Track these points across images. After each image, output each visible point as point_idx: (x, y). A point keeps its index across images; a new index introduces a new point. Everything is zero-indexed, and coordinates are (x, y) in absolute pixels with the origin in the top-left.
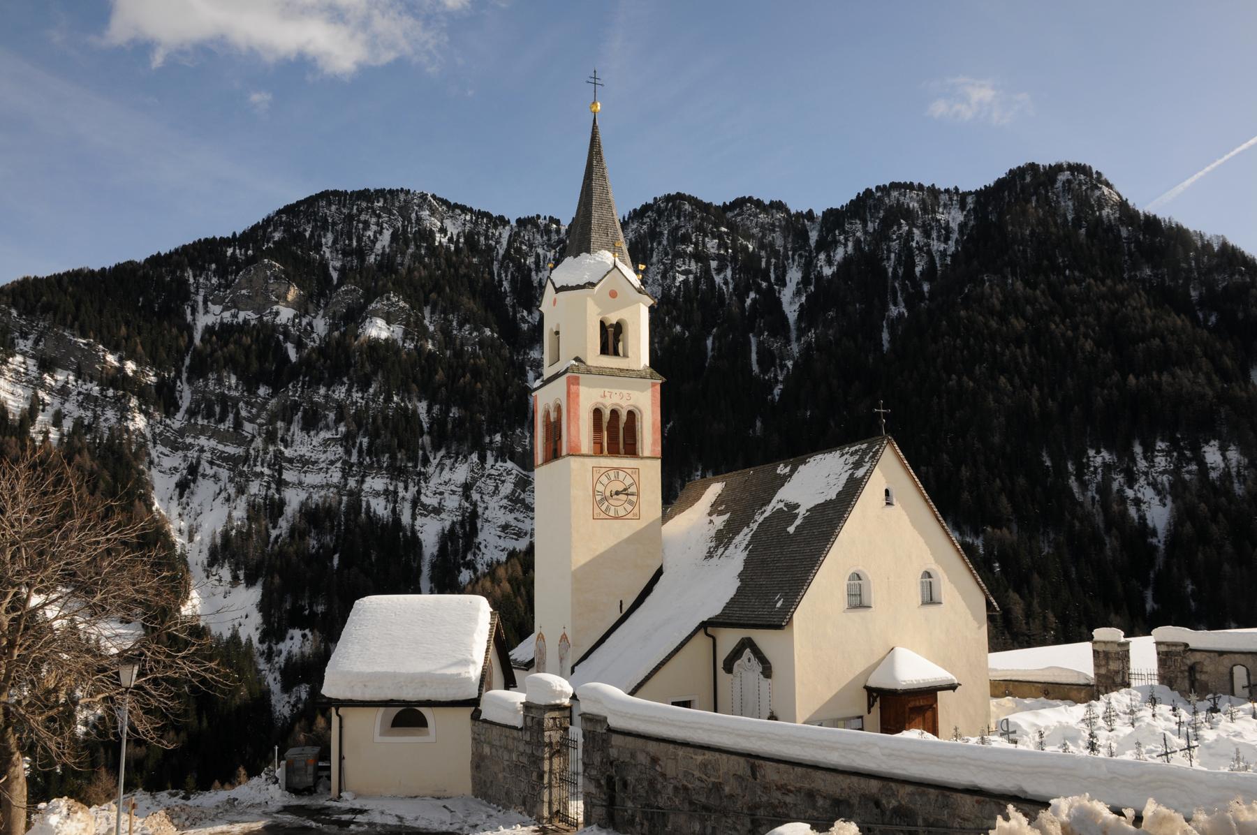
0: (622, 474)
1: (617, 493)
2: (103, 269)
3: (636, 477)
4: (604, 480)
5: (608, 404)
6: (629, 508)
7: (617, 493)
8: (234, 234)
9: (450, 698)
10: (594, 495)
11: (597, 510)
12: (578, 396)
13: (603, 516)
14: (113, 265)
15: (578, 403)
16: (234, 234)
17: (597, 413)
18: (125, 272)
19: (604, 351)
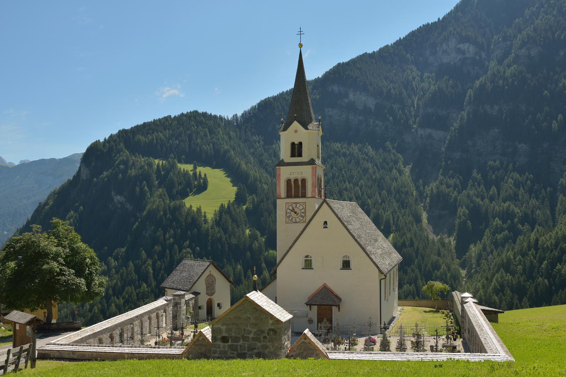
0: (298, 205)
1: (296, 213)
2: (374, 52)
3: (304, 206)
4: (301, 207)
5: (292, 177)
6: (301, 218)
7: (296, 213)
8: (439, 19)
9: (379, 287)
10: (286, 214)
11: (287, 220)
12: (280, 175)
13: (290, 222)
14: (378, 49)
15: (280, 178)
16: (439, 19)
17: (289, 181)
18: (385, 51)
19: (293, 155)
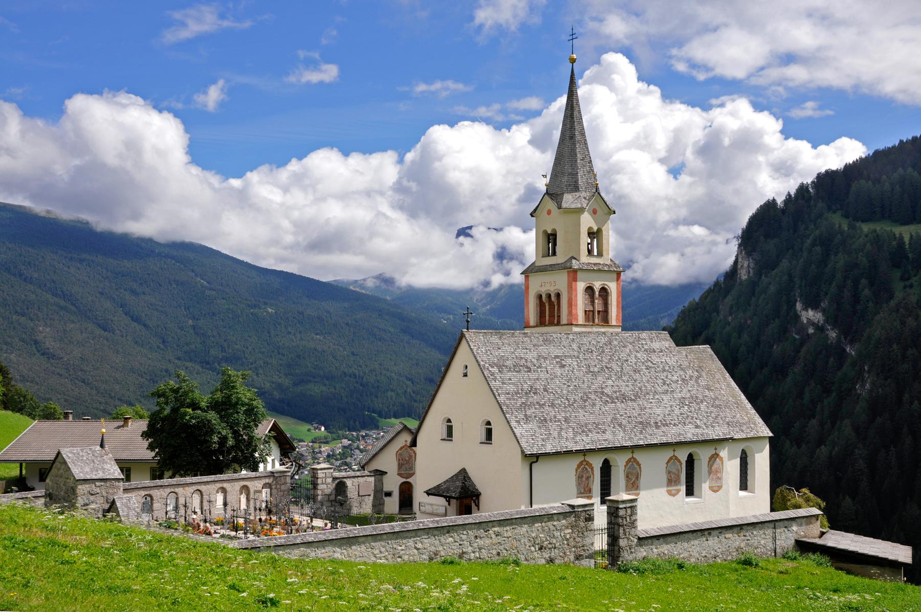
5: (543, 290)
